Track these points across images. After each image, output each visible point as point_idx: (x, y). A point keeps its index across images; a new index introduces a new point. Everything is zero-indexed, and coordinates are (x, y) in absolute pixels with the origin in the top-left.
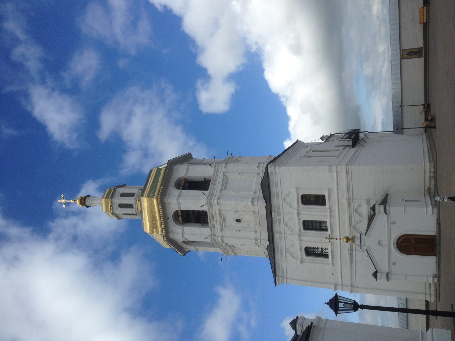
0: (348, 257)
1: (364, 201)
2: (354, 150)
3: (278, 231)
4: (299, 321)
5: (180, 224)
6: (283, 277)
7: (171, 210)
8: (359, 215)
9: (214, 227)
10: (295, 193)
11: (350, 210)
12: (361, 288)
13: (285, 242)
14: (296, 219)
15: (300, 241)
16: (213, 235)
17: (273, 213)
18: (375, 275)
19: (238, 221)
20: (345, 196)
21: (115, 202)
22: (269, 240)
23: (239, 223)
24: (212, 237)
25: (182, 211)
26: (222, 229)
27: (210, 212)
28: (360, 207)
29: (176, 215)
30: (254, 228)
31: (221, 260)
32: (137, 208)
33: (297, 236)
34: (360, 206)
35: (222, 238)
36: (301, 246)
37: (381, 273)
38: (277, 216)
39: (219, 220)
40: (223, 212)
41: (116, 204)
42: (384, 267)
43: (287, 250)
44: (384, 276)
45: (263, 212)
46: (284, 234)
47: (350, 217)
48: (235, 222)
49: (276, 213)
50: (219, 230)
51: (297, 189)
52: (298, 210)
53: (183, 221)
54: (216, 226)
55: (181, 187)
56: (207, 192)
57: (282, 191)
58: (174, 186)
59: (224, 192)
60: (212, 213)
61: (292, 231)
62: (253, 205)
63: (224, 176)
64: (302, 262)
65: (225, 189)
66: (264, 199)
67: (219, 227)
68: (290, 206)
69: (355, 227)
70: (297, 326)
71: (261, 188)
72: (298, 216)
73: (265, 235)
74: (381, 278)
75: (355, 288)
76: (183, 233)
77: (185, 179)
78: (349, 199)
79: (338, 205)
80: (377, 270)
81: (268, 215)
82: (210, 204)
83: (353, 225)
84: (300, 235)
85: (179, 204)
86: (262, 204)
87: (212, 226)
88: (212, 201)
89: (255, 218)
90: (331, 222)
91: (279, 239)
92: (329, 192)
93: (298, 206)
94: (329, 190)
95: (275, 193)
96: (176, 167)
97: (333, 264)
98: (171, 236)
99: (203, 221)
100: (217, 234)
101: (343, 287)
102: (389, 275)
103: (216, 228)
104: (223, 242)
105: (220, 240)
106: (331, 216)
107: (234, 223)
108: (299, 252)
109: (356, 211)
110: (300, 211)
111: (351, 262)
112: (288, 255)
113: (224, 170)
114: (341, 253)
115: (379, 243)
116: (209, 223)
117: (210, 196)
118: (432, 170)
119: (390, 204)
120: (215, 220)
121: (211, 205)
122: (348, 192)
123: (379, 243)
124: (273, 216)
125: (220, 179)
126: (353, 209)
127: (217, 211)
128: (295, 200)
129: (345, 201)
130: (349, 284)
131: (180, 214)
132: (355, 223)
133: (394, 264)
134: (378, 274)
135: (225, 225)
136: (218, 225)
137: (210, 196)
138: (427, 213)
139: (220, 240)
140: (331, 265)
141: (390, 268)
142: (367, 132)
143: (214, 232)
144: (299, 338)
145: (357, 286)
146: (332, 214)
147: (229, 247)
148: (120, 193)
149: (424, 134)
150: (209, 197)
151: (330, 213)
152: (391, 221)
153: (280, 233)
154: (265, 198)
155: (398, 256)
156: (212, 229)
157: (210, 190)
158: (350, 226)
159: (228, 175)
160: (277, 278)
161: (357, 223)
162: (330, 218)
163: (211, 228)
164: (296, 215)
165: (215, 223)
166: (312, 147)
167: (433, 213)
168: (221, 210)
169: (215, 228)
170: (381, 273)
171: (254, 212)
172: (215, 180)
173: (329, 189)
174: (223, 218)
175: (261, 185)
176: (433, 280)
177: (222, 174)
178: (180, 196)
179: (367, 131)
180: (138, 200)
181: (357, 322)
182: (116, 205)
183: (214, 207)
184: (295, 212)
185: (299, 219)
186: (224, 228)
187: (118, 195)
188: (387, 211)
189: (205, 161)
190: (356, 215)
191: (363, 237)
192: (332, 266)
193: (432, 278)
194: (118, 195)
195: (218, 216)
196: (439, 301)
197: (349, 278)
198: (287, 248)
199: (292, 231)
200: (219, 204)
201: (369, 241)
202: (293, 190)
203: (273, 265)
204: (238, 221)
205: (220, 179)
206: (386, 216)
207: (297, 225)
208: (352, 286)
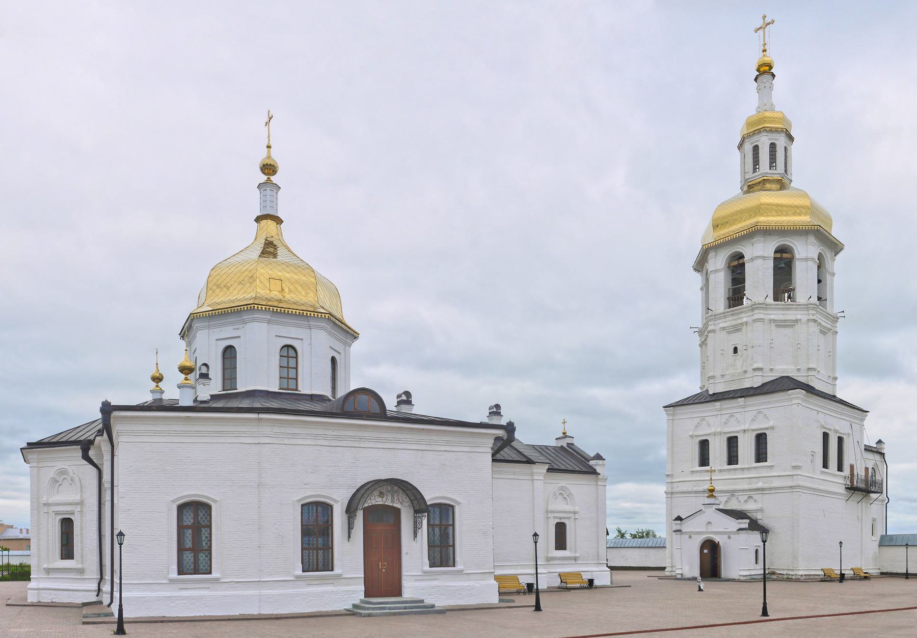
1: (760, 506)
2: (842, 490)
3: (723, 407)
4: (600, 462)
5: (729, 264)
6: (673, 415)
7: (744, 248)
8: (746, 500)
10: (767, 426)
11: (750, 490)
12: (671, 502)
14: (738, 429)
15: (715, 434)
16: (716, 317)
17: (743, 399)
18: (679, 518)
19: (735, 350)
20: (766, 486)
21: (760, 138)
22: (714, 394)
23: (733, 352)
24: (714, 317)
25: (743, 264)
26: (723, 329)
27: (743, 310)
30: (728, 373)
32: (753, 179)
33: (719, 430)
34: (755, 501)
35: (713, 330)
36: (709, 434)
37: (681, 524)
38: (740, 404)
39: (734, 323)
40: (744, 328)
41: (758, 141)
42: (686, 527)
43: (703, 419)
44: (678, 528)
45: (747, 384)
46: (721, 414)
47: (744, 491)
48: (734, 346)
49: (742, 404)
50: (722, 325)
51: (772, 428)
52: (748, 430)
54: (727, 319)
55: (778, 255)
56: (770, 300)
58: (779, 244)
59: (773, 325)
60: (742, 312)
61: (726, 423)
62: (754, 370)
63: (797, 321)
64: (692, 436)
65: (776, 325)
67: (725, 325)
68: (753, 420)
69: (733, 495)
70: (596, 461)
72: (741, 430)
73: (720, 388)
74: (676, 524)
75: (670, 496)
76: (716, 271)
77: (793, 258)
78: (763, 489)
79: (756, 478)
80: (683, 521)
81: (742, 391)
82: (754, 307)
83: (735, 494)
84: (721, 433)
85: (752, 259)
86: (756, 381)
87: (727, 314)
89: (739, 373)
90: (737, 469)
91: (715, 408)
92: (770, 466)
93: (753, 430)
94: (771, 467)
95: (766, 401)
96: (812, 239)
97: (693, 472)
98: (711, 255)
100: (717, 322)
101: (670, 484)
102: (679, 533)
103: (724, 320)
104: (709, 332)
105: (710, 328)
106: (743, 469)
108: (703, 432)
109: (750, 497)
110: (747, 433)
111: (696, 492)
112: (698, 420)
113: (804, 318)
114: (704, 480)
115: (709, 523)
116: (732, 309)
117: (764, 306)
118: (794, 577)
120: (735, 317)
121: (753, 310)
122: (770, 489)
123: (709, 523)
124: (739, 399)
125: (791, 315)
127: (745, 320)
128: (760, 425)
129: (760, 485)
130: (674, 490)
131: (741, 261)
133: (690, 537)
134: (679, 522)
135: (729, 333)
136: (728, 322)
137: (764, 306)
138: (740, 570)
139: (710, 328)
140: (691, 470)
141: (686, 533)
142: (887, 501)
143: (720, 318)
145: (673, 498)
146: (745, 470)
147: (706, 340)
148: (776, 142)
149: (880, 571)
150: (762, 306)
151: (747, 468)
152: (692, 535)
153: (721, 410)
154: (764, 385)
155: (698, 541)
156: (722, 315)
157: (775, 305)
158: (734, 491)
159: (798, 326)
160: (672, 408)
161: (738, 498)
162: (741, 469)
163: (724, 313)
164: (743, 428)
165: (730, 318)
166: (849, 435)
167: (740, 576)
168: (746, 325)
170: (681, 524)
171: (745, 372)
172: (790, 308)
173: (773, 466)
174: (737, 329)
175: (782, 377)
176: (678, 574)
177: (799, 317)
178: (764, 259)
179: (888, 502)
180: (765, 178)
181: (124, 617)
182: (756, 141)
183: (750, 314)
184: (746, 427)
185: (738, 432)
186: (725, 331)
187: (772, 139)
188: (741, 531)
189: (828, 276)
190: (746, 498)
191: (715, 507)
192: (691, 471)
193: (681, 572)
194: (772, 139)
195: (739, 321)
196: (659, 579)
197: (679, 489)
198: (705, 418)
199: (726, 423)
200: (755, 321)
201: (710, 514)
202: (771, 424)
203: (680, 403)
204: (735, 350)
205: (791, 315)
206: (735, 530)
207: (733, 428)
208: (672, 493)
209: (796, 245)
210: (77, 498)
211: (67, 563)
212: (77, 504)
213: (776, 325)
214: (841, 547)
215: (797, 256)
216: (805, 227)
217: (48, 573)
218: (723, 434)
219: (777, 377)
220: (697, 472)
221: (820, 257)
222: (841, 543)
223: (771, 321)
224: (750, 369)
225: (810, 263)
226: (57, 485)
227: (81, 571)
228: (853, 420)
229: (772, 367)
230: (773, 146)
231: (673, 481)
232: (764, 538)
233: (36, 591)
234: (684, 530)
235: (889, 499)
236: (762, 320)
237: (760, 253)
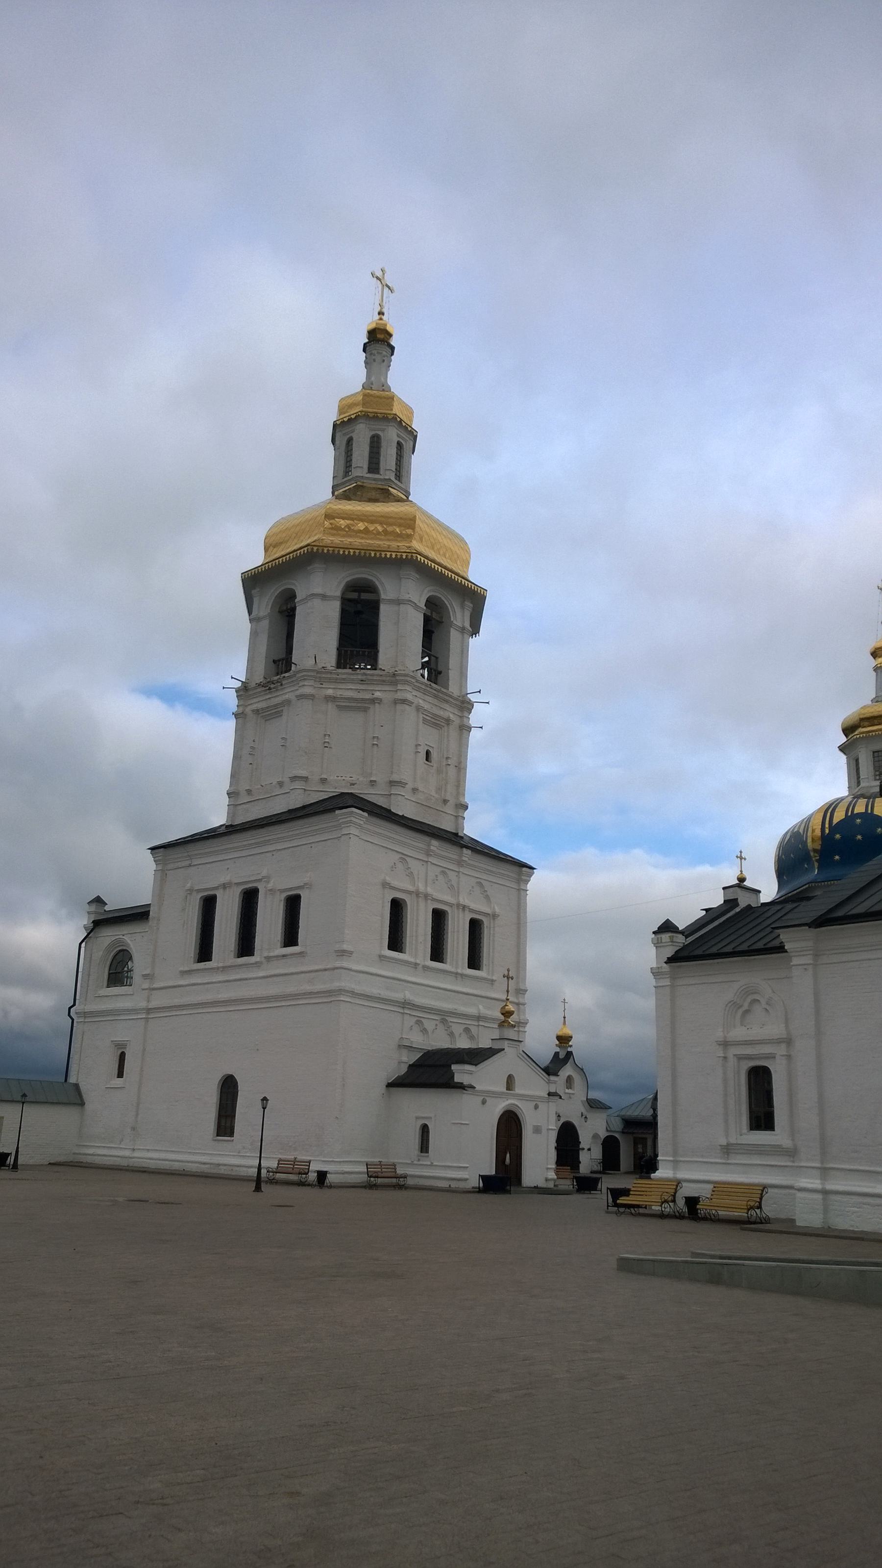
0: (398, 996)
9: (425, 694)
13: (418, 859)
28: (422, 1029)
29: (368, 588)
31: (224, 688)
53: (350, 600)
54: (427, 698)
55: (354, 595)
57: (492, 884)
58: (354, 577)
63: (373, 701)
66: (303, 806)
71: (339, 793)
88: (311, 683)
99: (355, 652)
107: (426, 745)
119: (527, 1100)
120: (436, 702)
126: (424, 1018)
127: (378, 694)
132: (450, 1024)
133: (484, 1102)
144: (738, 910)
152: (487, 1098)
169: (422, 694)
179: (70, 1008)
207: (443, 896)
209: (382, 583)
210: (776, 1029)
211: (762, 1137)
212: (779, 1041)
213: (337, 705)
214: (264, 1108)
215: (383, 596)
216: (344, 551)
217: (728, 1155)
218: (194, 893)
219: (335, 794)
220: (426, 968)
221: (432, 603)
222: (265, 1099)
223: (329, 699)
224: (286, 780)
225: (410, 610)
226: (740, 1012)
227: (792, 1153)
228: (485, 877)
229: (324, 776)
230: (375, 444)
231: (155, 986)
232: (265, 1105)
233: (603, 1183)
234: (478, 1087)
235: (69, 1015)
236: (311, 697)
237: (318, 590)
